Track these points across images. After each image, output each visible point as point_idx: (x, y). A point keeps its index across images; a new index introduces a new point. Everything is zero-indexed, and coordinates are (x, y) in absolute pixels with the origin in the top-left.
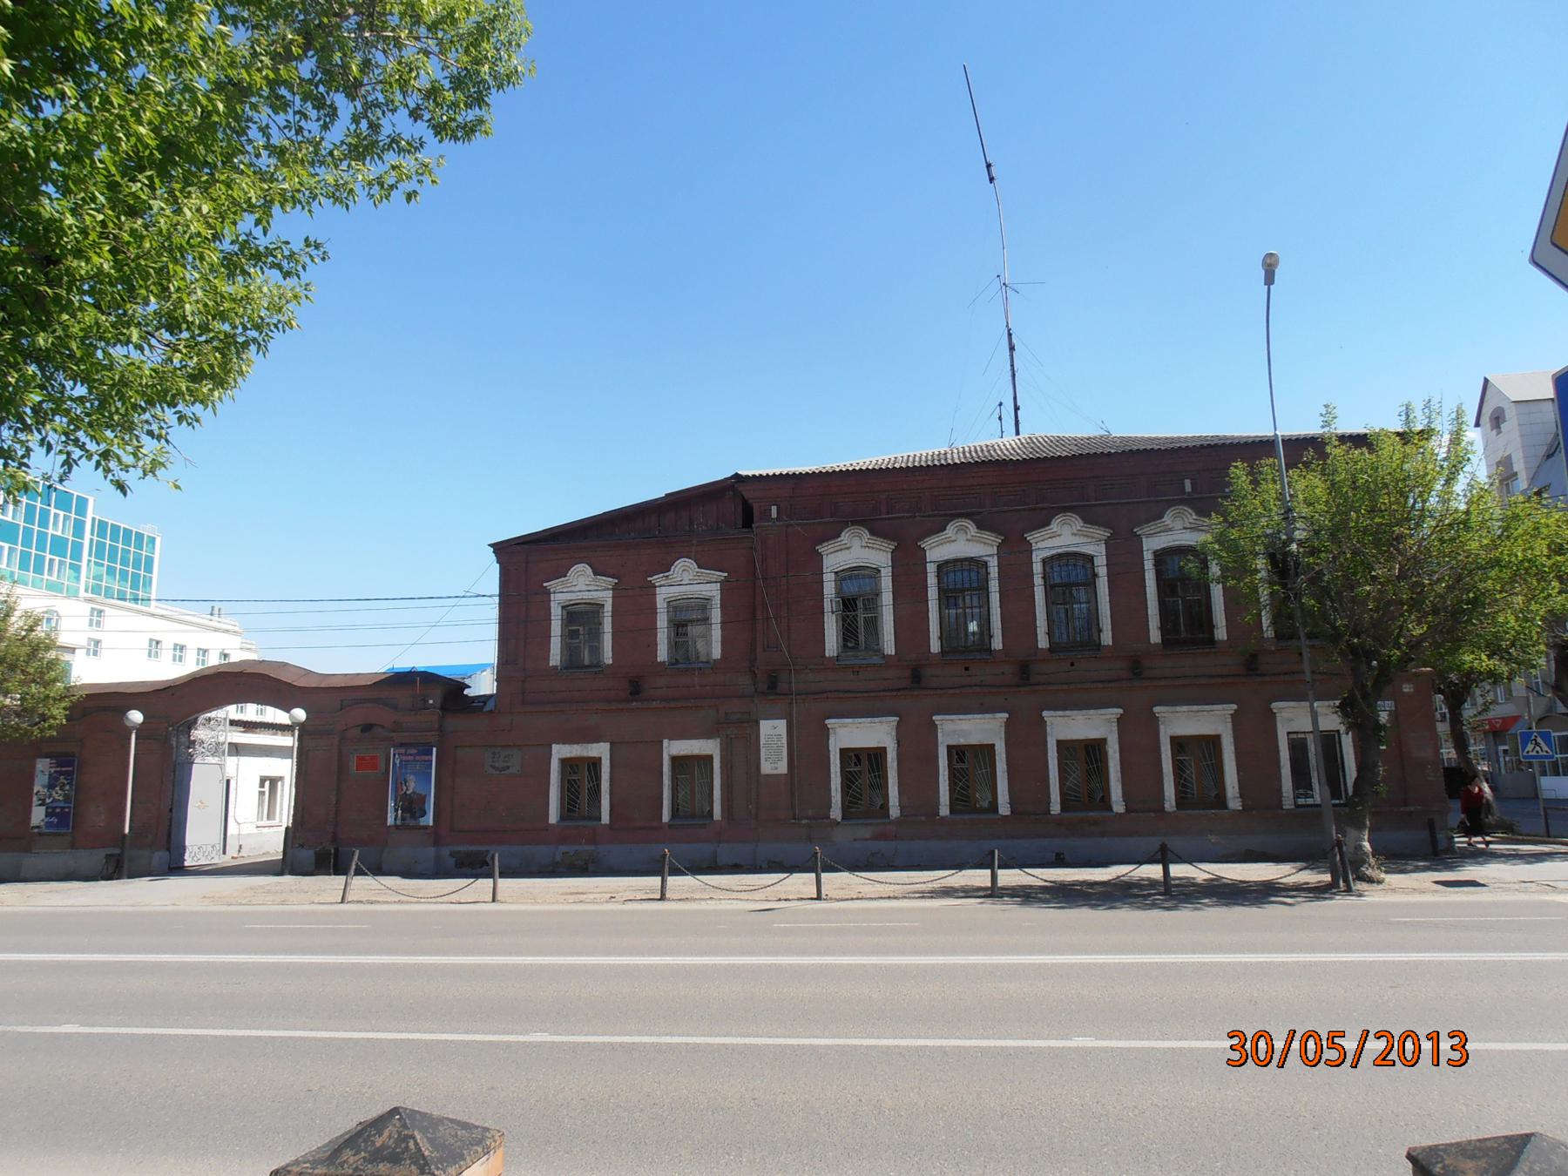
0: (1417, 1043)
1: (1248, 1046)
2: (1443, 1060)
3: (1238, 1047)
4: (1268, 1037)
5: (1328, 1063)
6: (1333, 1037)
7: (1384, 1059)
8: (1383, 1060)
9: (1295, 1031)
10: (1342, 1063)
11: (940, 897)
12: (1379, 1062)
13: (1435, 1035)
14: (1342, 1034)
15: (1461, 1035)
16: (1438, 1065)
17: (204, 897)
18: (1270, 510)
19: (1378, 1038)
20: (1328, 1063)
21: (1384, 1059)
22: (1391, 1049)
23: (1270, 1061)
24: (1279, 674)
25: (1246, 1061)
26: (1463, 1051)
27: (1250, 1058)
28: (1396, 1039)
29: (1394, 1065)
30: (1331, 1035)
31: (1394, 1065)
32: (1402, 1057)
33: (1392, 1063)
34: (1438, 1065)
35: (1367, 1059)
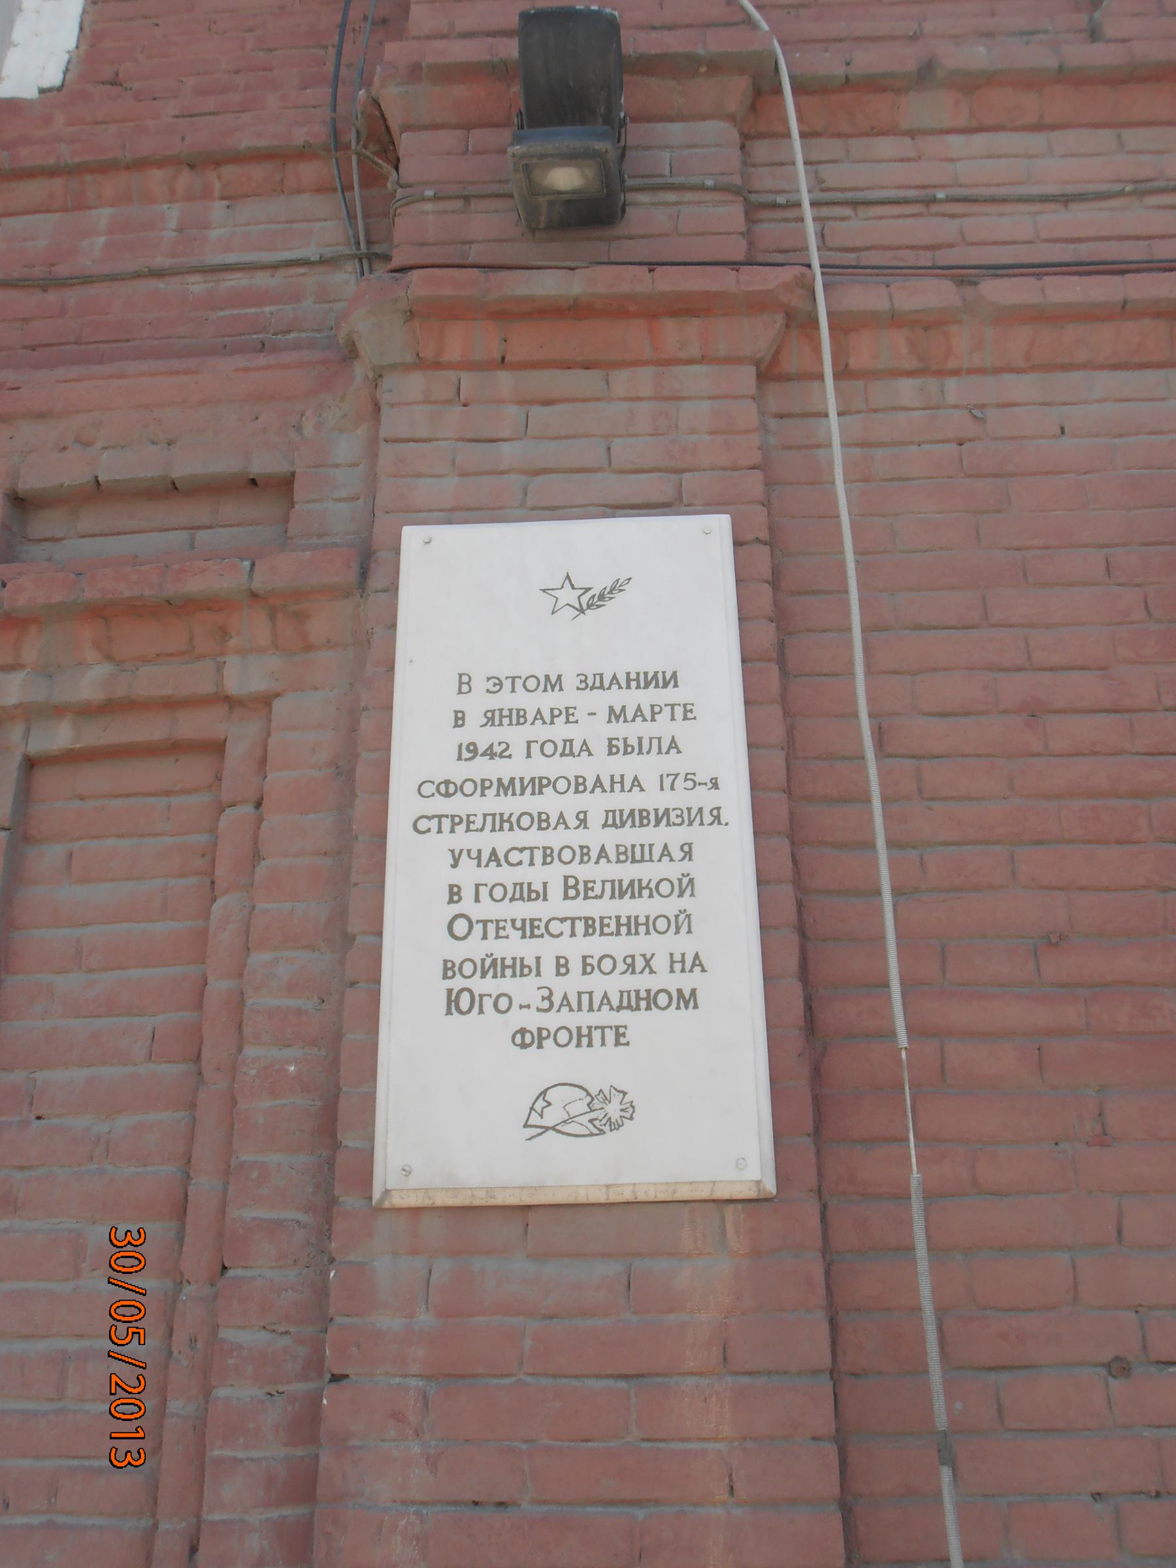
0: (133, 1270)
1: (129, 1248)
2: (116, 1443)
3: (129, 1238)
4: (137, 1416)
5: (114, 1328)
6: (139, 1333)
7: (117, 1384)
8: (116, 1386)
9: (145, 1295)
10: (113, 1342)
11: (605, 516)
12: (114, 1378)
13: (141, 1435)
14: (142, 1342)
15: (141, 1461)
16: (111, 1438)
17: (123, 447)
18: (348, 147)
19: (138, 1378)
20: (114, 1328)
21: (117, 1384)
22: (127, 1391)
23: (114, 1270)
24: (990, 186)
25: (114, 1246)
26: (125, 1243)
27: (118, 1250)
28: (137, 1396)
29: (111, 1394)
30: (142, 1331)
31: (111, 1394)
32: (119, 1402)
33: (113, 1391)
34: (111, 1438)
35: (117, 1367)
